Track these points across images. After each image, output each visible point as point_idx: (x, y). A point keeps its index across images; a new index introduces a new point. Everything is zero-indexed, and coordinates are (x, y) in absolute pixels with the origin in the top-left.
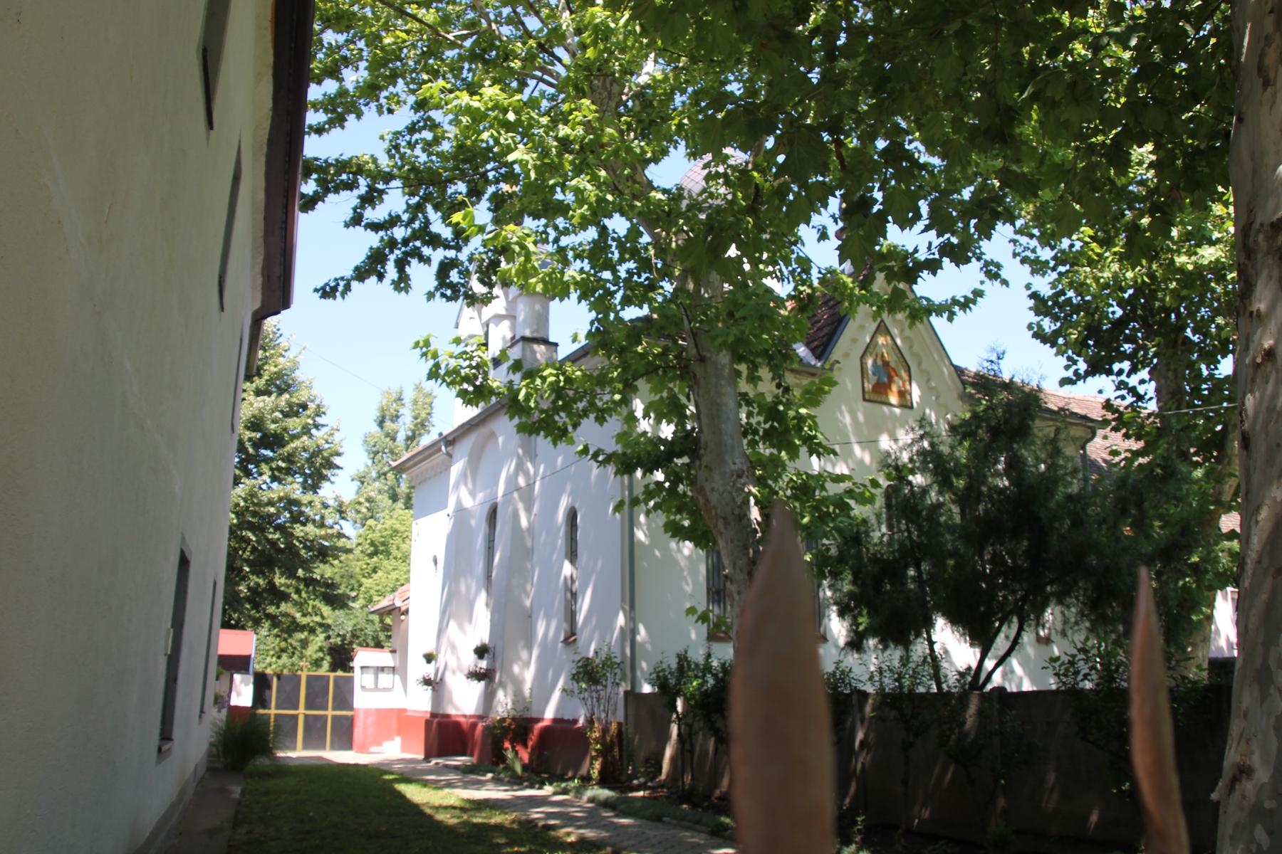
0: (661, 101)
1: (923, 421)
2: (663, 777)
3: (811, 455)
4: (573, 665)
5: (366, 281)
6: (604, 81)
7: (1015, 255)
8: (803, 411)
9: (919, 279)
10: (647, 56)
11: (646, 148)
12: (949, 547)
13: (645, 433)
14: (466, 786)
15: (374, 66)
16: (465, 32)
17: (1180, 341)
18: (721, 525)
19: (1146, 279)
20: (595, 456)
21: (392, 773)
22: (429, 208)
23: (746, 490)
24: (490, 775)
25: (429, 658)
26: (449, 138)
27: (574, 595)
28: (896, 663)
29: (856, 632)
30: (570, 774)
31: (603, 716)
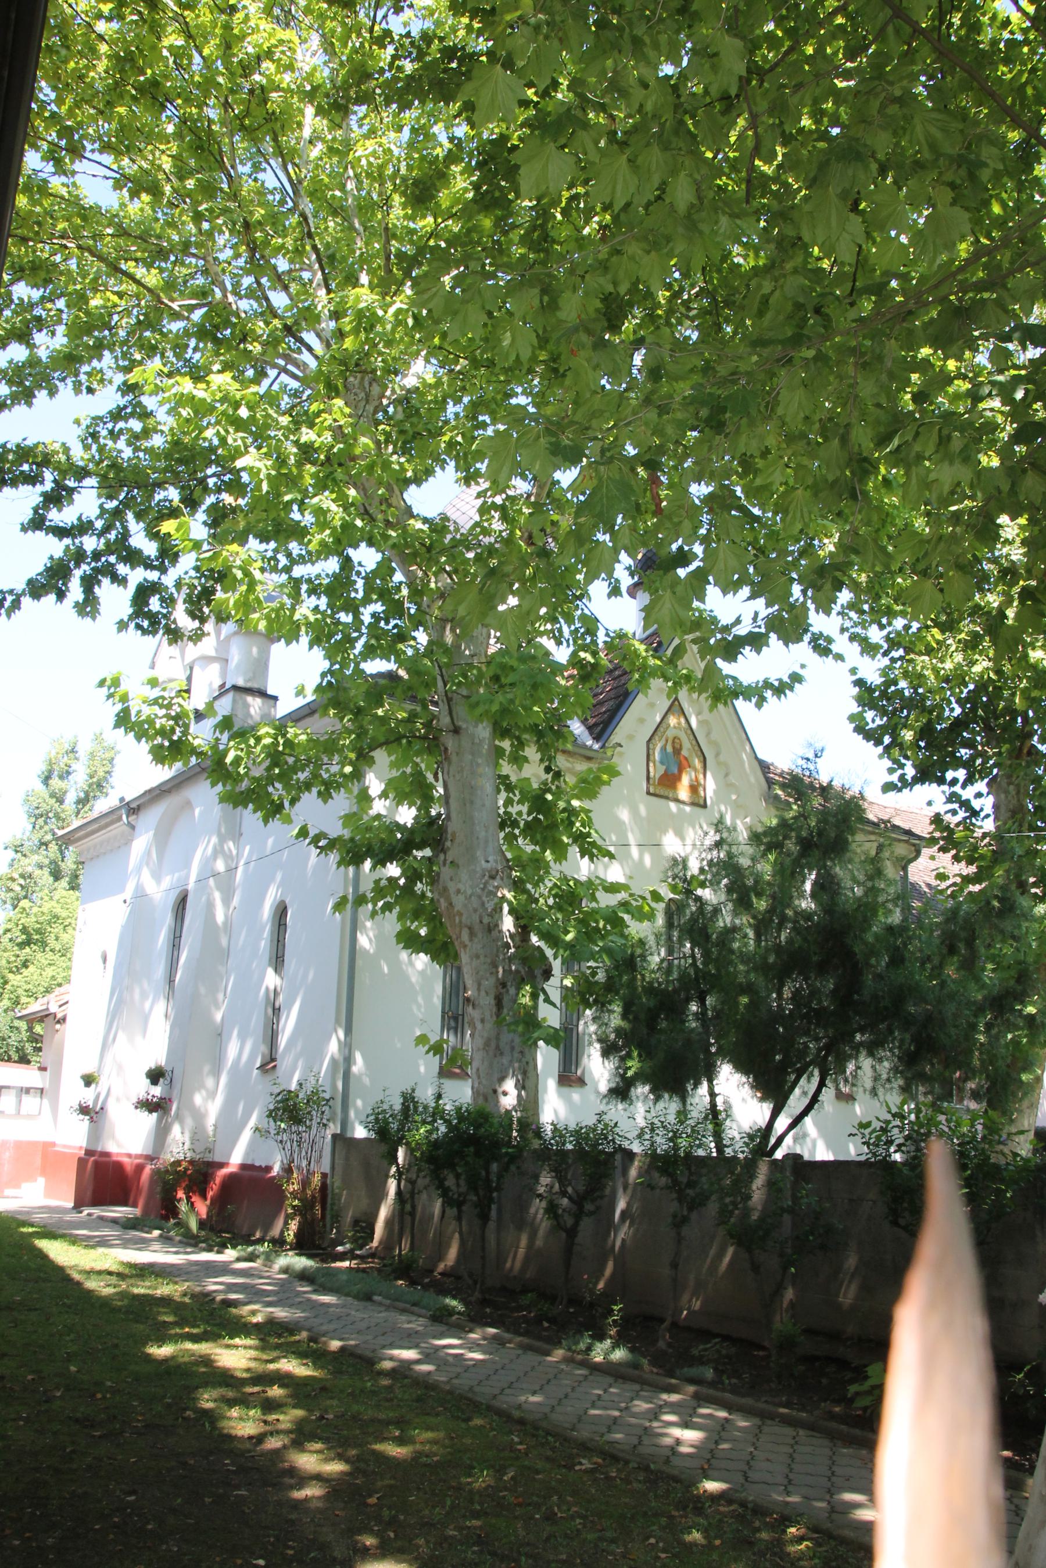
0: (430, 409)
1: (719, 825)
2: (375, 1243)
3: (582, 857)
4: (271, 1099)
5: (43, 599)
6: (362, 379)
8: (575, 803)
9: (740, 656)
10: (418, 353)
11: (407, 465)
12: (741, 979)
13: (379, 816)
14: (126, 1244)
15: (77, 331)
16: (194, 302)
17: (1025, 751)
18: (465, 936)
19: (992, 675)
20: (315, 840)
21: (32, 1226)
22: (130, 516)
23: (499, 894)
24: (156, 1233)
25: (89, 1080)
26: (162, 432)
27: (276, 1011)
28: (672, 1118)
29: (623, 1076)
30: (258, 1235)
31: (304, 1163)
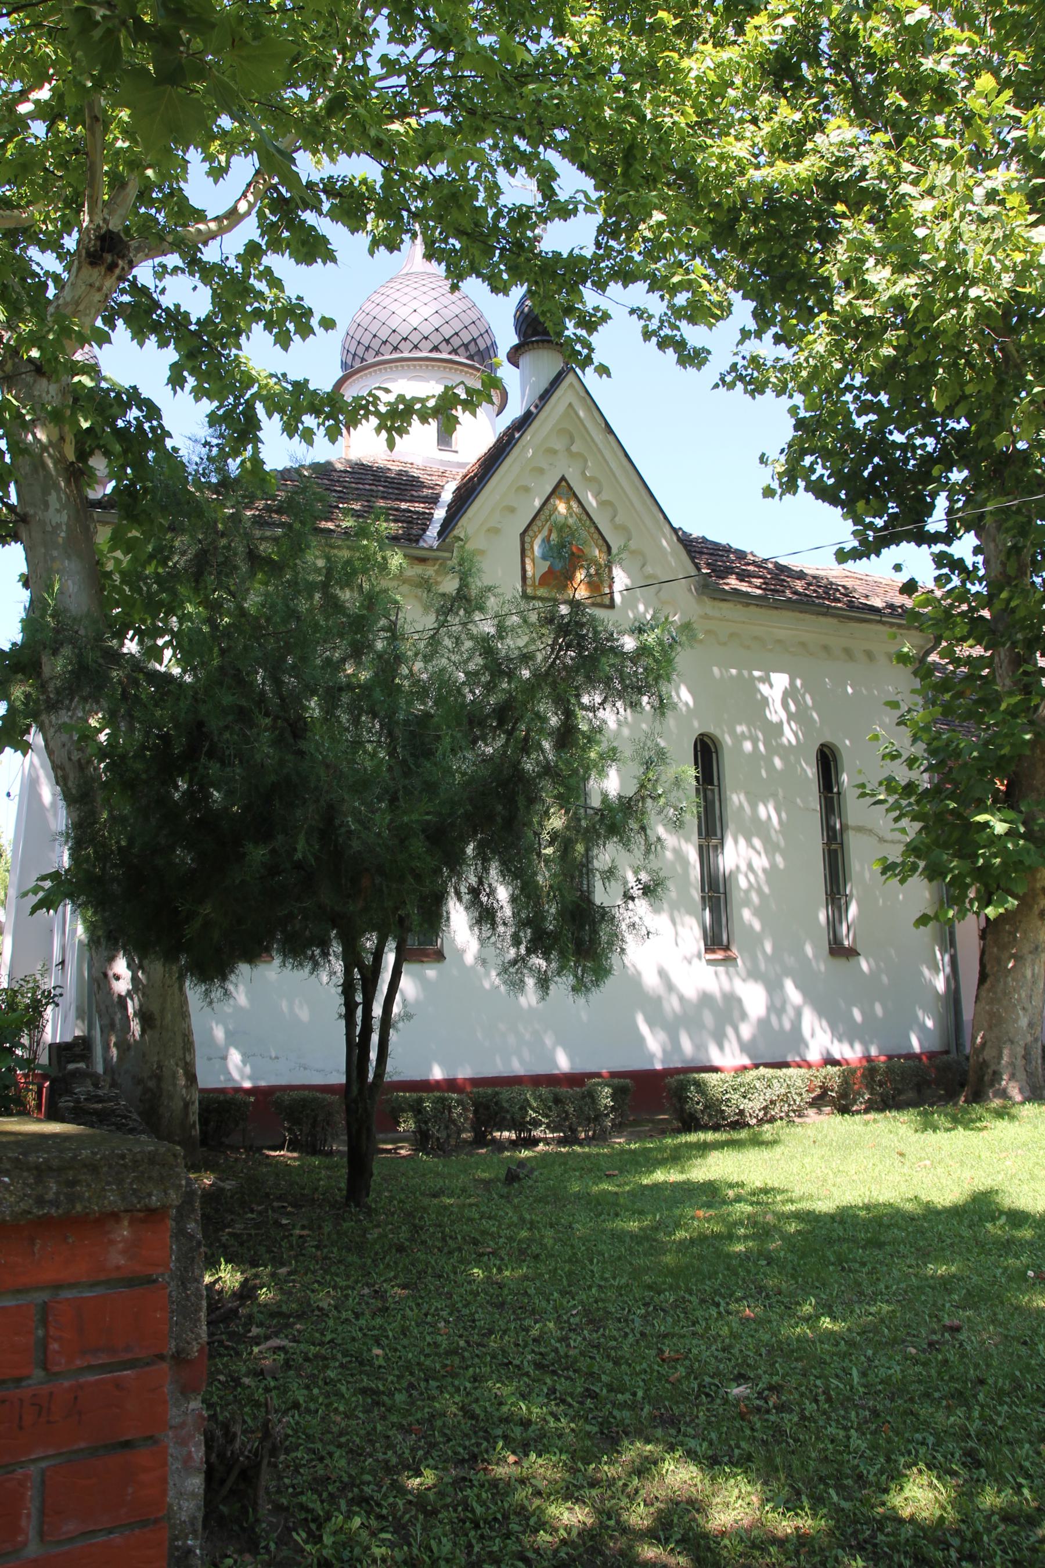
7: (647, 335)
